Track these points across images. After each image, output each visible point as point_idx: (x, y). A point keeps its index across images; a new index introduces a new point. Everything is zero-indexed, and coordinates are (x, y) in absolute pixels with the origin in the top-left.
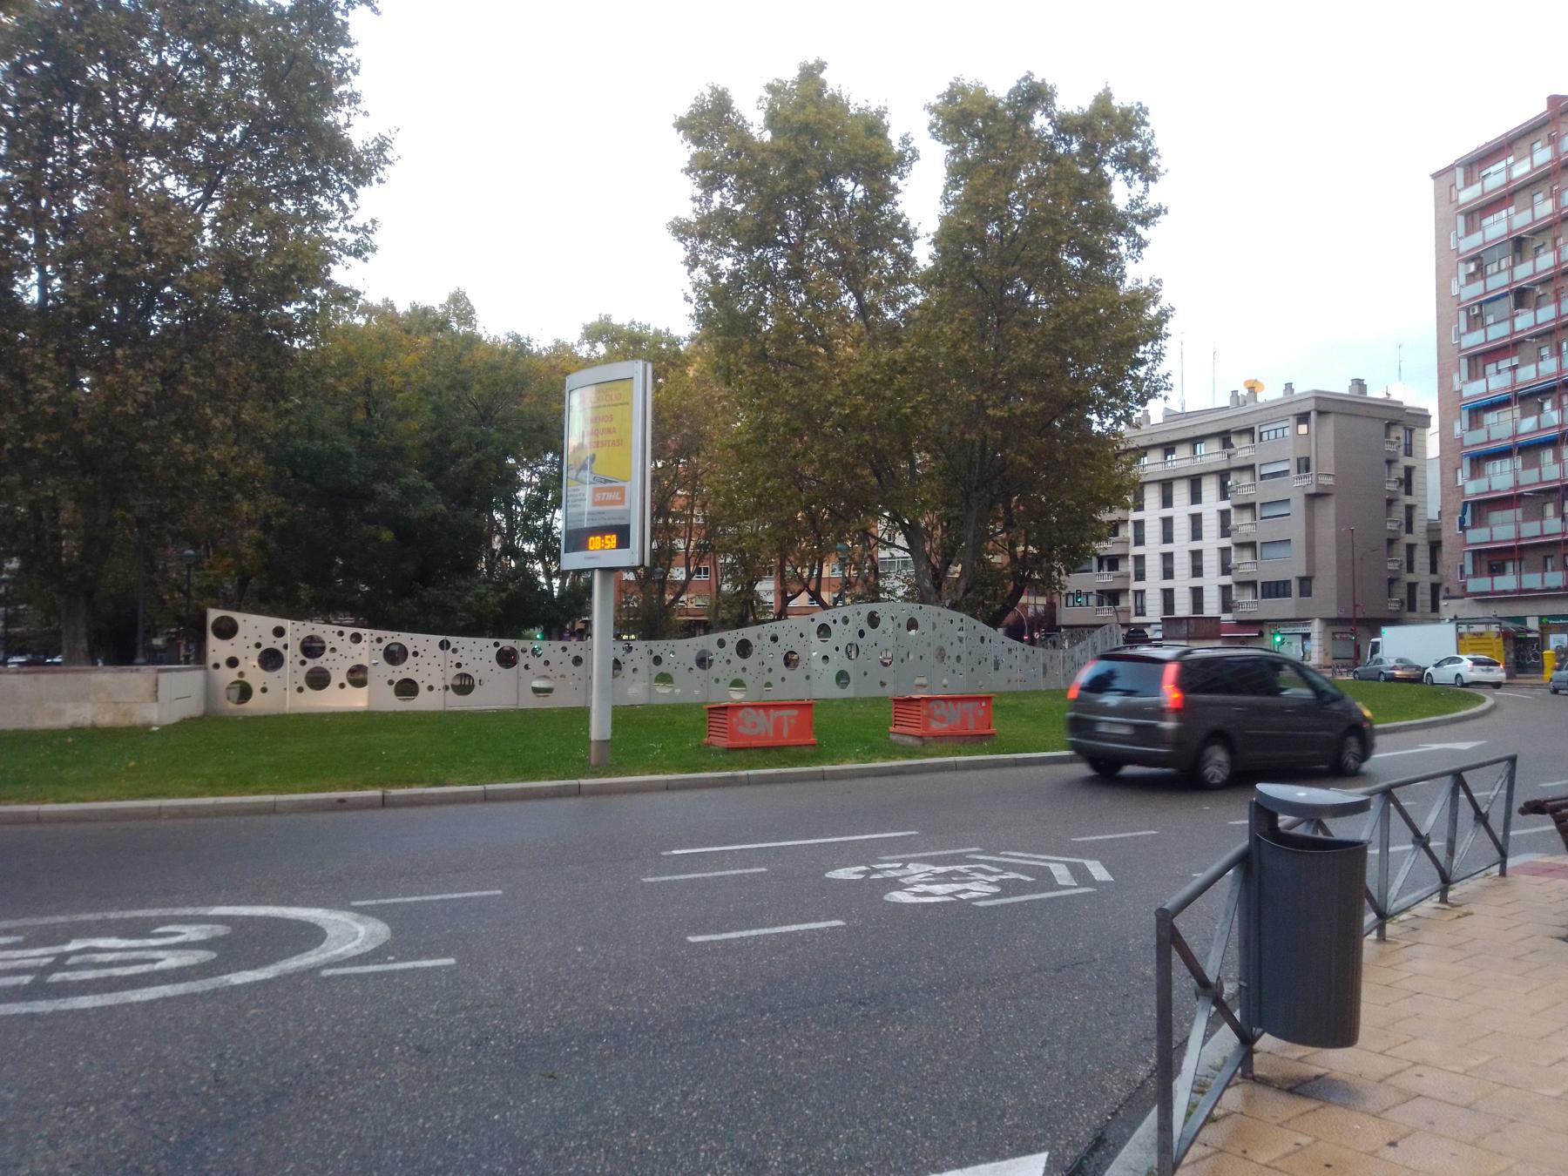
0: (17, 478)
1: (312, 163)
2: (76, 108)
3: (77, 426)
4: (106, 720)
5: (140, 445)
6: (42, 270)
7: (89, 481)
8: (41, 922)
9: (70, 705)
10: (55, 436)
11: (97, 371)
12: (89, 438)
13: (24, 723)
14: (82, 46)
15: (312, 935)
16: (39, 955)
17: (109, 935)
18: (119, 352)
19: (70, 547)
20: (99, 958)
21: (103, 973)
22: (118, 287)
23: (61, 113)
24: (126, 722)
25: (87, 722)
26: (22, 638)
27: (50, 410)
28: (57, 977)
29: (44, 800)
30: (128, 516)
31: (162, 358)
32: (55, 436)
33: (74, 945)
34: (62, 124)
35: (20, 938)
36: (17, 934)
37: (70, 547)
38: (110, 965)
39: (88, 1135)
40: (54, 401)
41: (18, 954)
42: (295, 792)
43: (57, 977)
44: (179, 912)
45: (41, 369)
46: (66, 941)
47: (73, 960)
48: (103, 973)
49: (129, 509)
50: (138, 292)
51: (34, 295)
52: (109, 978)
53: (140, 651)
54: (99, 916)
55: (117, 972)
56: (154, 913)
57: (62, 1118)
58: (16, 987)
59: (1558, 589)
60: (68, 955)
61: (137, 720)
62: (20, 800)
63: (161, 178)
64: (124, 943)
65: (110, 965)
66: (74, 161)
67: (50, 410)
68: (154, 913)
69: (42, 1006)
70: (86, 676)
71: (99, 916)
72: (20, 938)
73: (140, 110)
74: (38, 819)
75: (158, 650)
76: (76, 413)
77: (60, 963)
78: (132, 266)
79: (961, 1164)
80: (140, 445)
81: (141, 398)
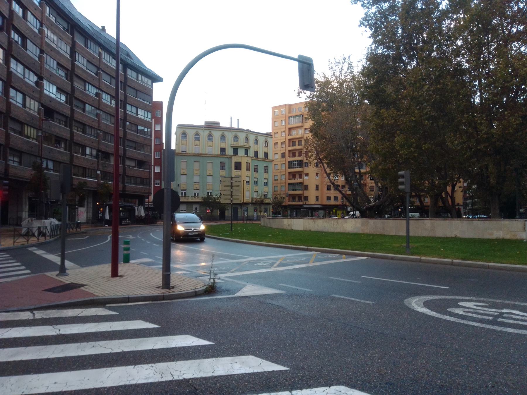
0: (476, 159)
1: (373, 53)
2: (489, 36)
3: (493, 140)
4: (508, 237)
5: (516, 143)
6: (480, 92)
7: (498, 157)
8: (493, 300)
9: (495, 231)
10: (487, 144)
11: (498, 120)
12: (498, 143)
13: (481, 236)
14: (490, 15)
15: (426, 304)
16: (493, 311)
17: (516, 310)
18: (506, 113)
19: (493, 181)
20: (514, 316)
21: (516, 322)
22: (506, 91)
23: (485, 39)
24: (514, 238)
25: (501, 237)
26: (477, 210)
27: (486, 136)
28: (500, 320)
29: (490, 261)
30: (511, 168)
31: (522, 111)
32: (487, 144)
33: (504, 311)
34: (485, 43)
35: (487, 305)
36: (486, 303)
37: (493, 181)
38: (518, 320)
39: (517, 375)
40: (486, 133)
41: (487, 309)
42: (441, 258)
43: (500, 320)
44: (464, 298)
45: (481, 124)
46: (502, 309)
47: (505, 315)
48: (516, 322)
49: (511, 165)
50: (512, 91)
51: (477, 100)
52: (518, 324)
53: (517, 214)
54: (512, 303)
55: (521, 323)
56: (457, 298)
57: (508, 367)
58: (488, 320)
59: (218, 155)
60: (504, 313)
61: (518, 237)
62: (479, 260)
63: (519, 49)
64: (522, 314)
65: (518, 320)
66: (490, 53)
67: (486, 136)
68: (457, 298)
69: (496, 328)
70: (498, 222)
71: (512, 303)
72: (487, 305)
73: (512, 27)
74: (488, 267)
75: (522, 213)
76: (493, 136)
77: (501, 315)
78: (509, 82)
79: (261, 393)
80: (516, 143)
81: (515, 126)
